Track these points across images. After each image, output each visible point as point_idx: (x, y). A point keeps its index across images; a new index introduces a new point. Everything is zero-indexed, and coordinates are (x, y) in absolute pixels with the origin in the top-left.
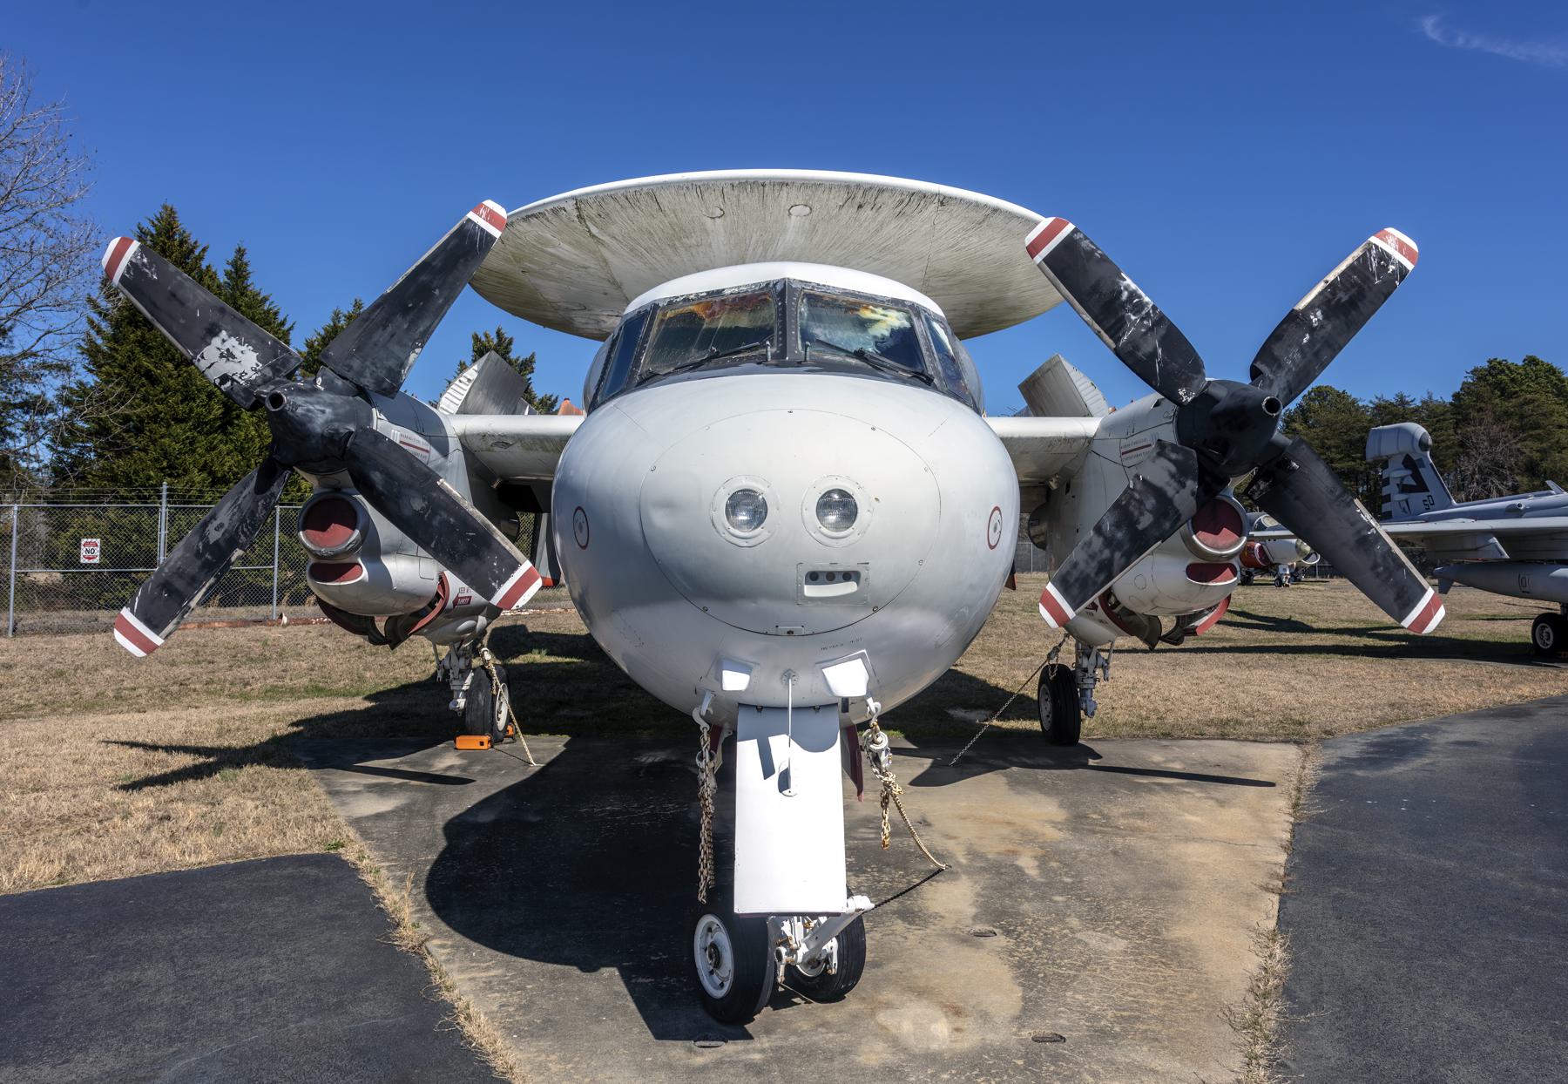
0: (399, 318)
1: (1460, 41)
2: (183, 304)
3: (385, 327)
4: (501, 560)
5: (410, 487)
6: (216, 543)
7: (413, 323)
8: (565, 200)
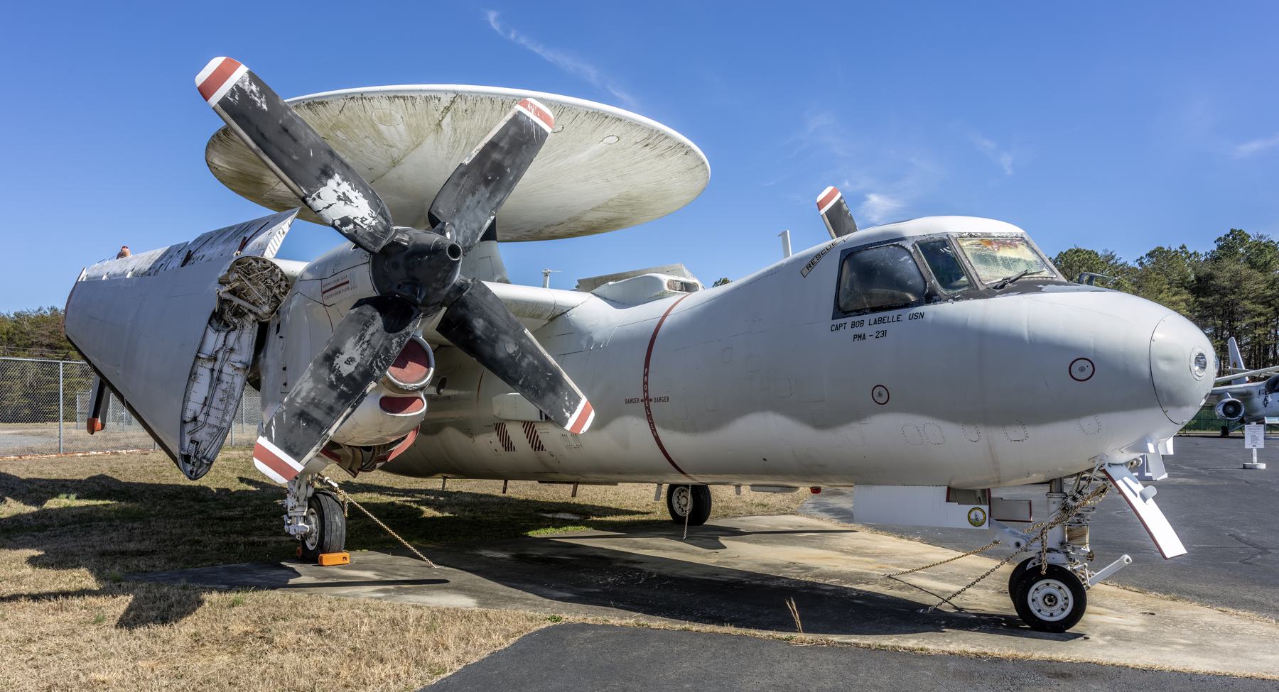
0: (483, 188)
1: (513, 36)
2: (295, 140)
3: (473, 194)
4: (569, 395)
5: (506, 333)
6: (350, 375)
7: (493, 194)
8: (446, 92)
